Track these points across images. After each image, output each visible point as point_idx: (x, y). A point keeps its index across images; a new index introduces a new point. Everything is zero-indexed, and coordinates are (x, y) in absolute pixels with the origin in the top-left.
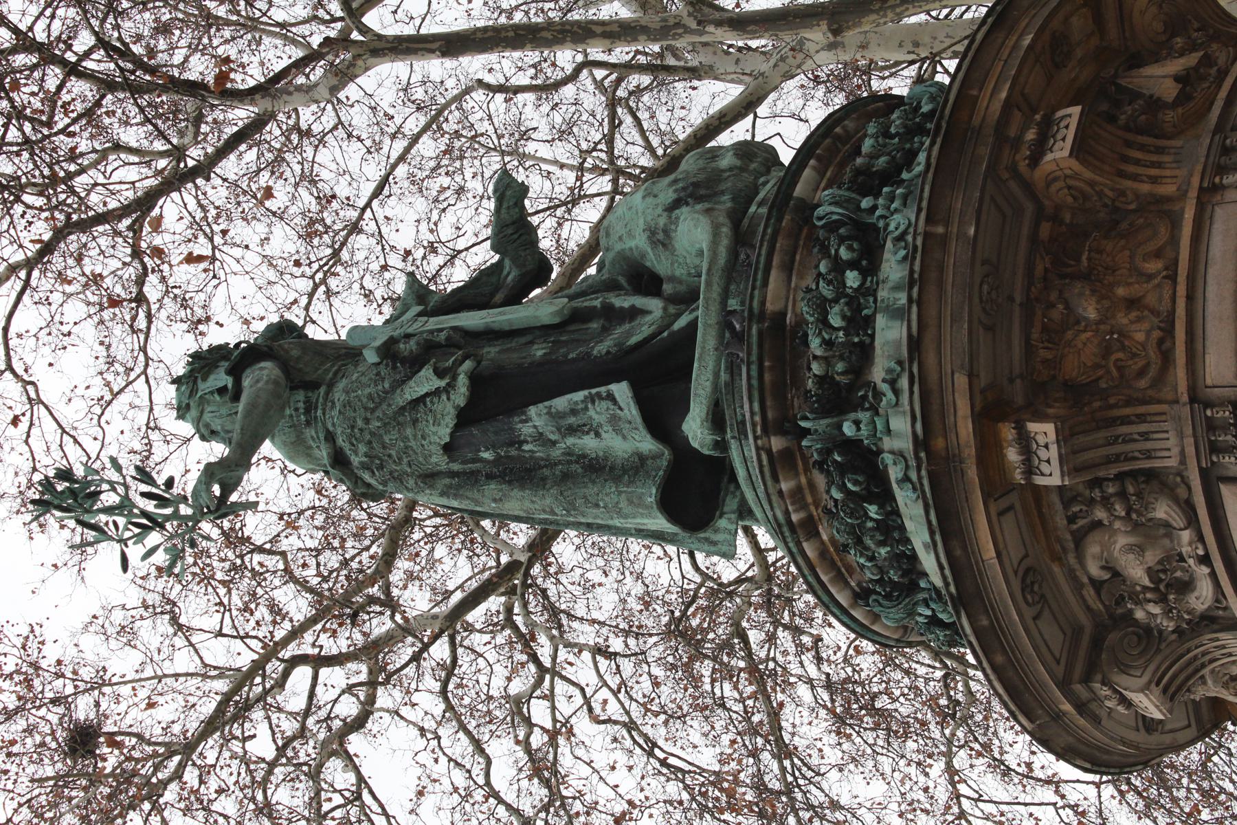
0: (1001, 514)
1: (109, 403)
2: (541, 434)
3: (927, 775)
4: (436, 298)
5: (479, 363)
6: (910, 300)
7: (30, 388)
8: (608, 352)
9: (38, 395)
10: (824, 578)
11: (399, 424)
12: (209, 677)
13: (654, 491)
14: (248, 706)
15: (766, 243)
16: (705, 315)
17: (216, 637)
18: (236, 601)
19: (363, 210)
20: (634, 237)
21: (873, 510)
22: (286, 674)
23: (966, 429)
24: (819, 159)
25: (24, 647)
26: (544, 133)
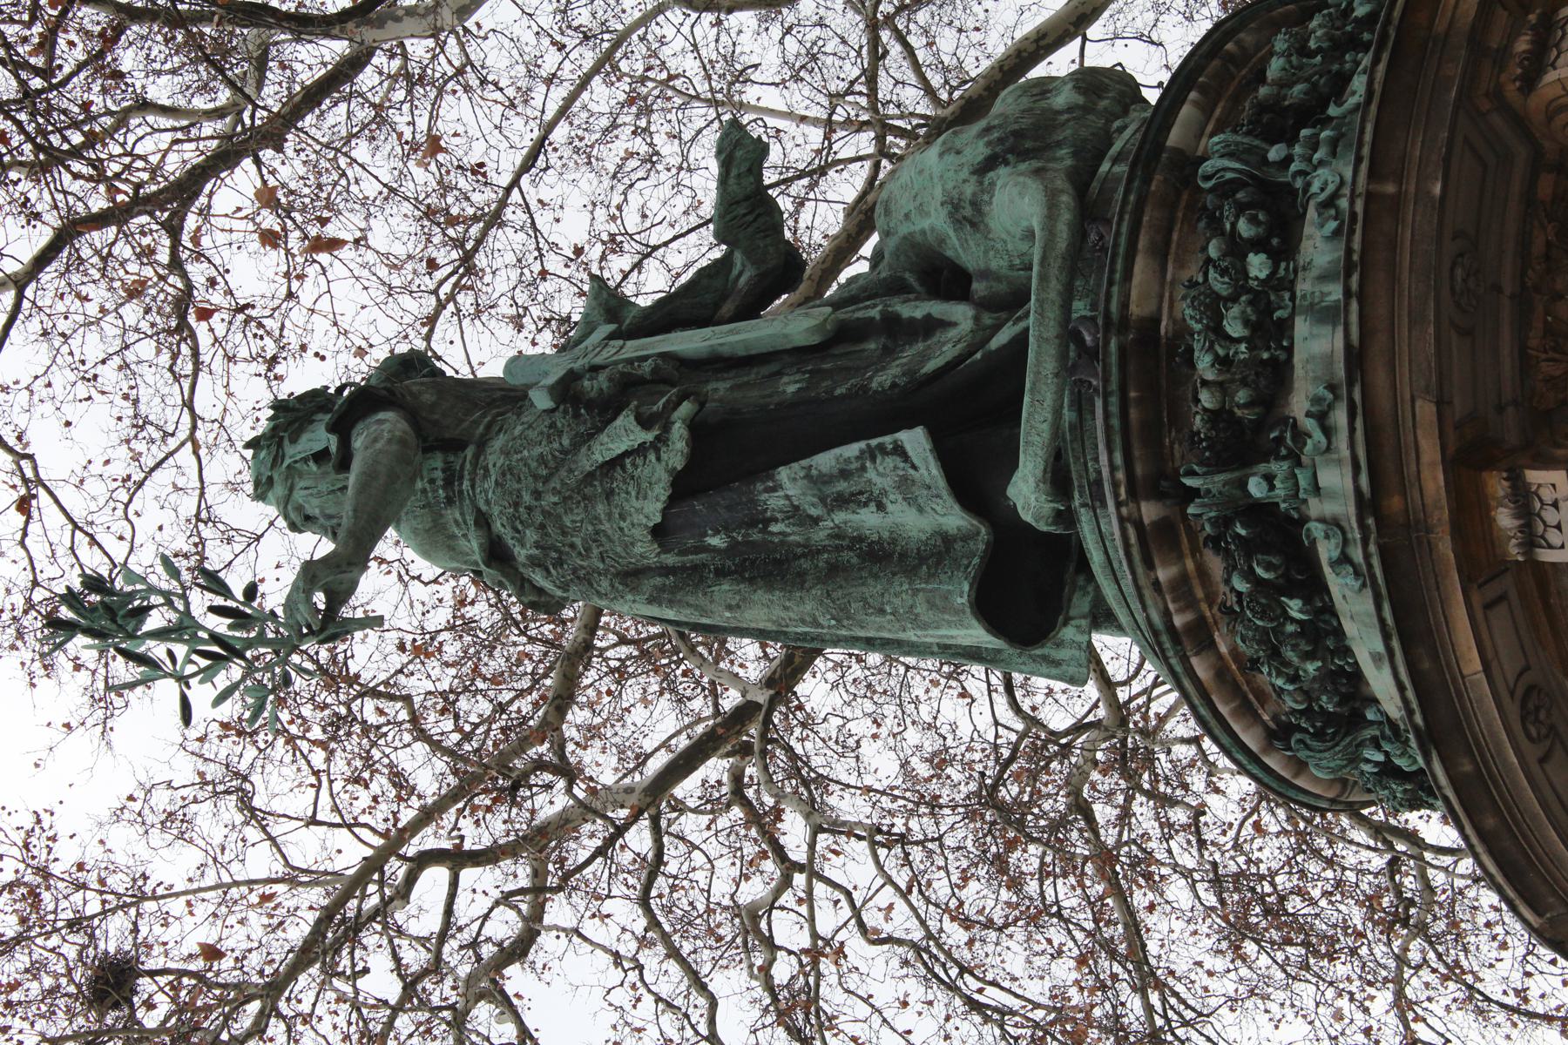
0: (1488, 606)
1: (140, 485)
2: (797, 508)
3: (1366, 1011)
4: (634, 312)
5: (702, 405)
6: (1347, 293)
7: (25, 464)
8: (894, 385)
9: (37, 474)
10: (1224, 710)
11: (585, 498)
12: (301, 884)
13: (966, 587)
14: (353, 932)
15: (1127, 217)
16: (1039, 326)
17: (307, 825)
18: (339, 766)
19: (508, 190)
20: (928, 214)
21: (1295, 607)
22: (411, 880)
23: (1434, 482)
24: (1203, 90)
25: (26, 846)
26: (771, 68)
